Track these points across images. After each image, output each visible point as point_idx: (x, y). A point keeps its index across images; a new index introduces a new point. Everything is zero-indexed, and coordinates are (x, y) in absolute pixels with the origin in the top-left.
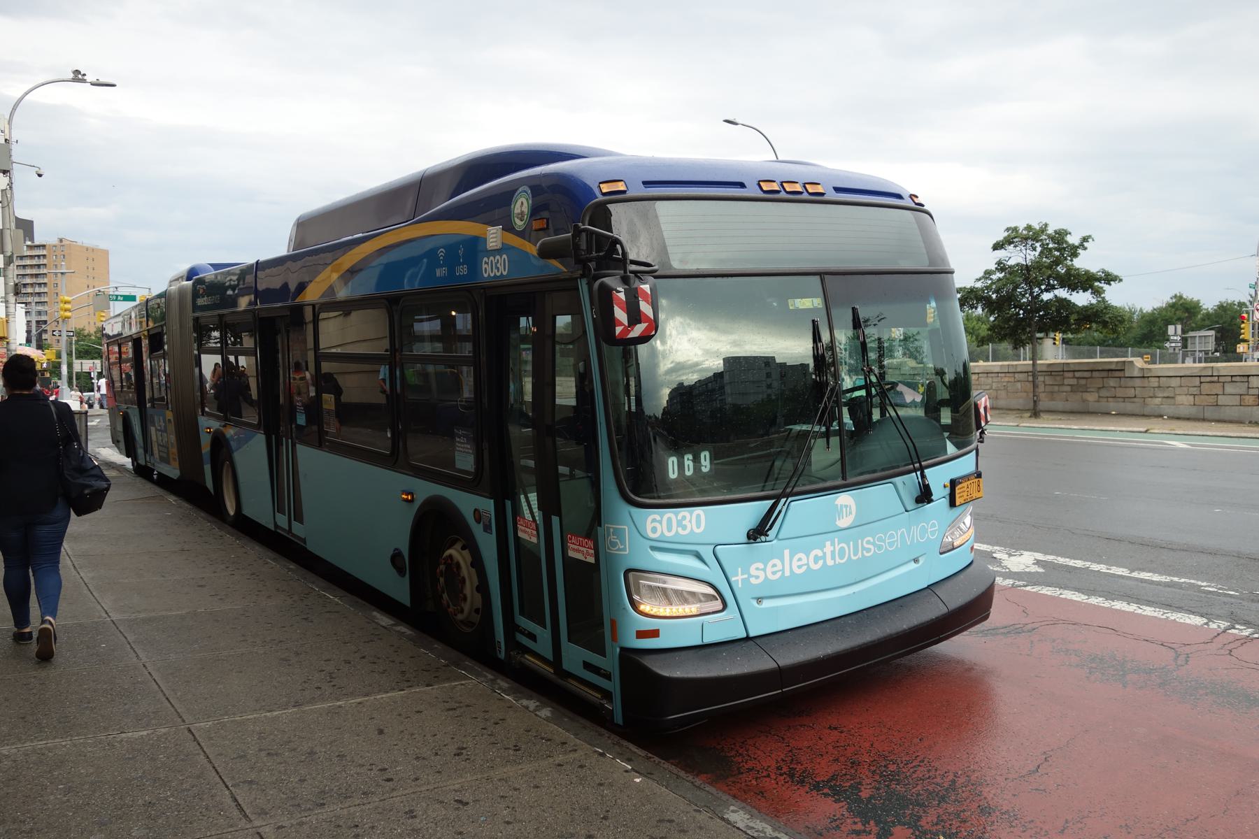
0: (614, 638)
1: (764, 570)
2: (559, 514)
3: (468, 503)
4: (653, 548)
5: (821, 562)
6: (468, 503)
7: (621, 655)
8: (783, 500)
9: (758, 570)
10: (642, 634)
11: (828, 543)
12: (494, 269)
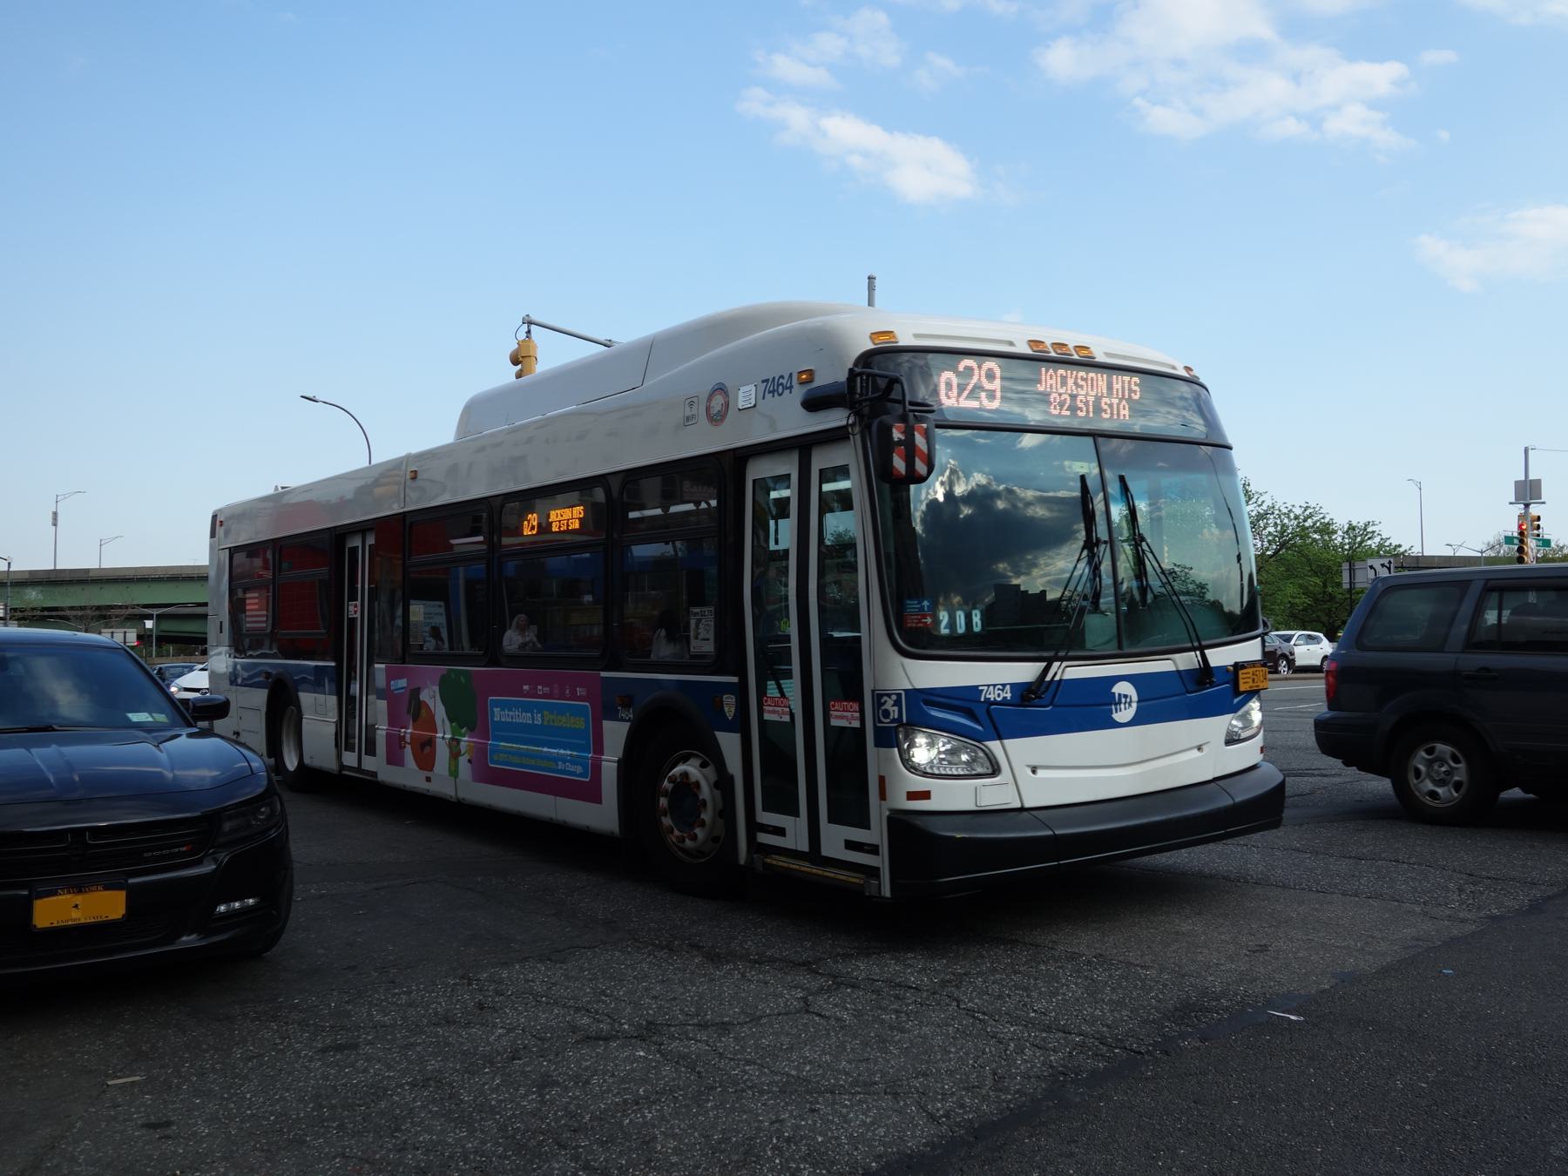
7: (889, 818)
8: (1056, 664)
10: (913, 796)
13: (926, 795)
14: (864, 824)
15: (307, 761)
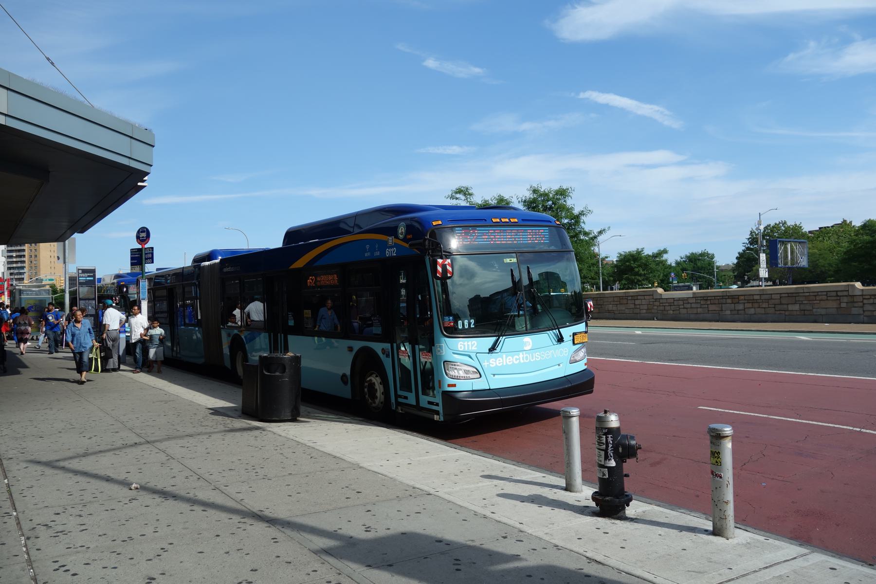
0: (440, 387)
3: (378, 347)
6: (378, 347)
9: (493, 362)
10: (449, 386)
12: (391, 252)
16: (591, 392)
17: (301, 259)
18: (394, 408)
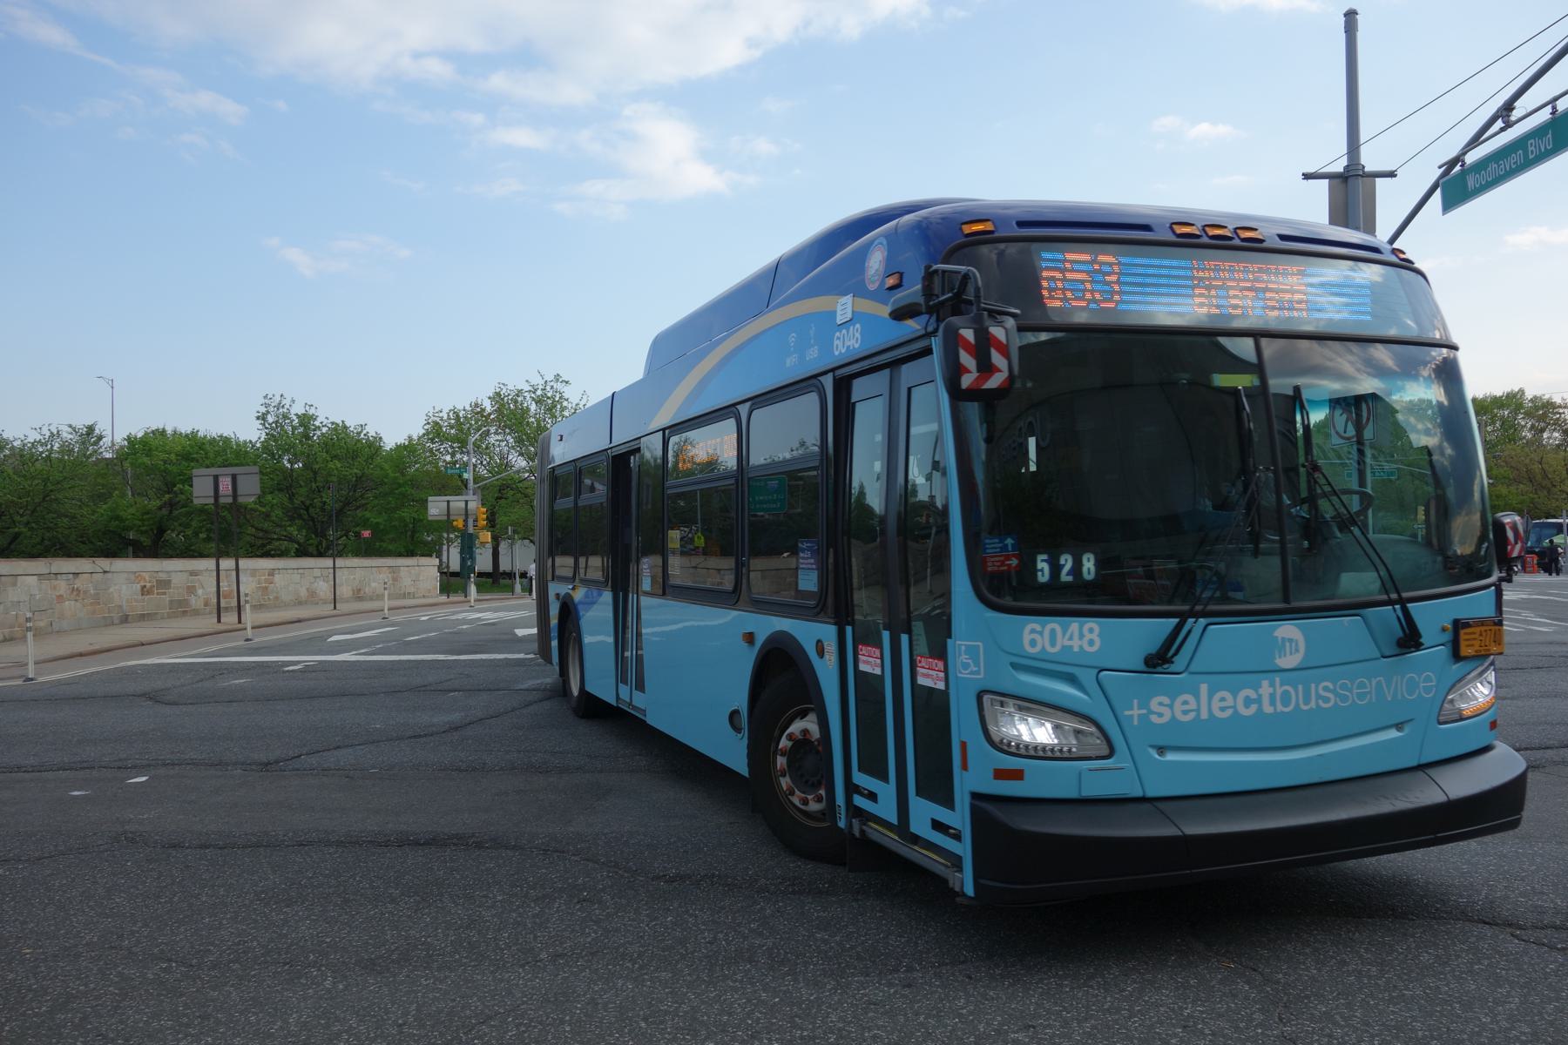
1: (1171, 707)
2: (909, 632)
3: (815, 635)
4: (1015, 666)
5: (1254, 708)
10: (1001, 774)
11: (1265, 683)
13: (1017, 775)
14: (948, 801)
15: (589, 688)
16: (1514, 824)
17: (1054, 624)
18: (842, 824)
